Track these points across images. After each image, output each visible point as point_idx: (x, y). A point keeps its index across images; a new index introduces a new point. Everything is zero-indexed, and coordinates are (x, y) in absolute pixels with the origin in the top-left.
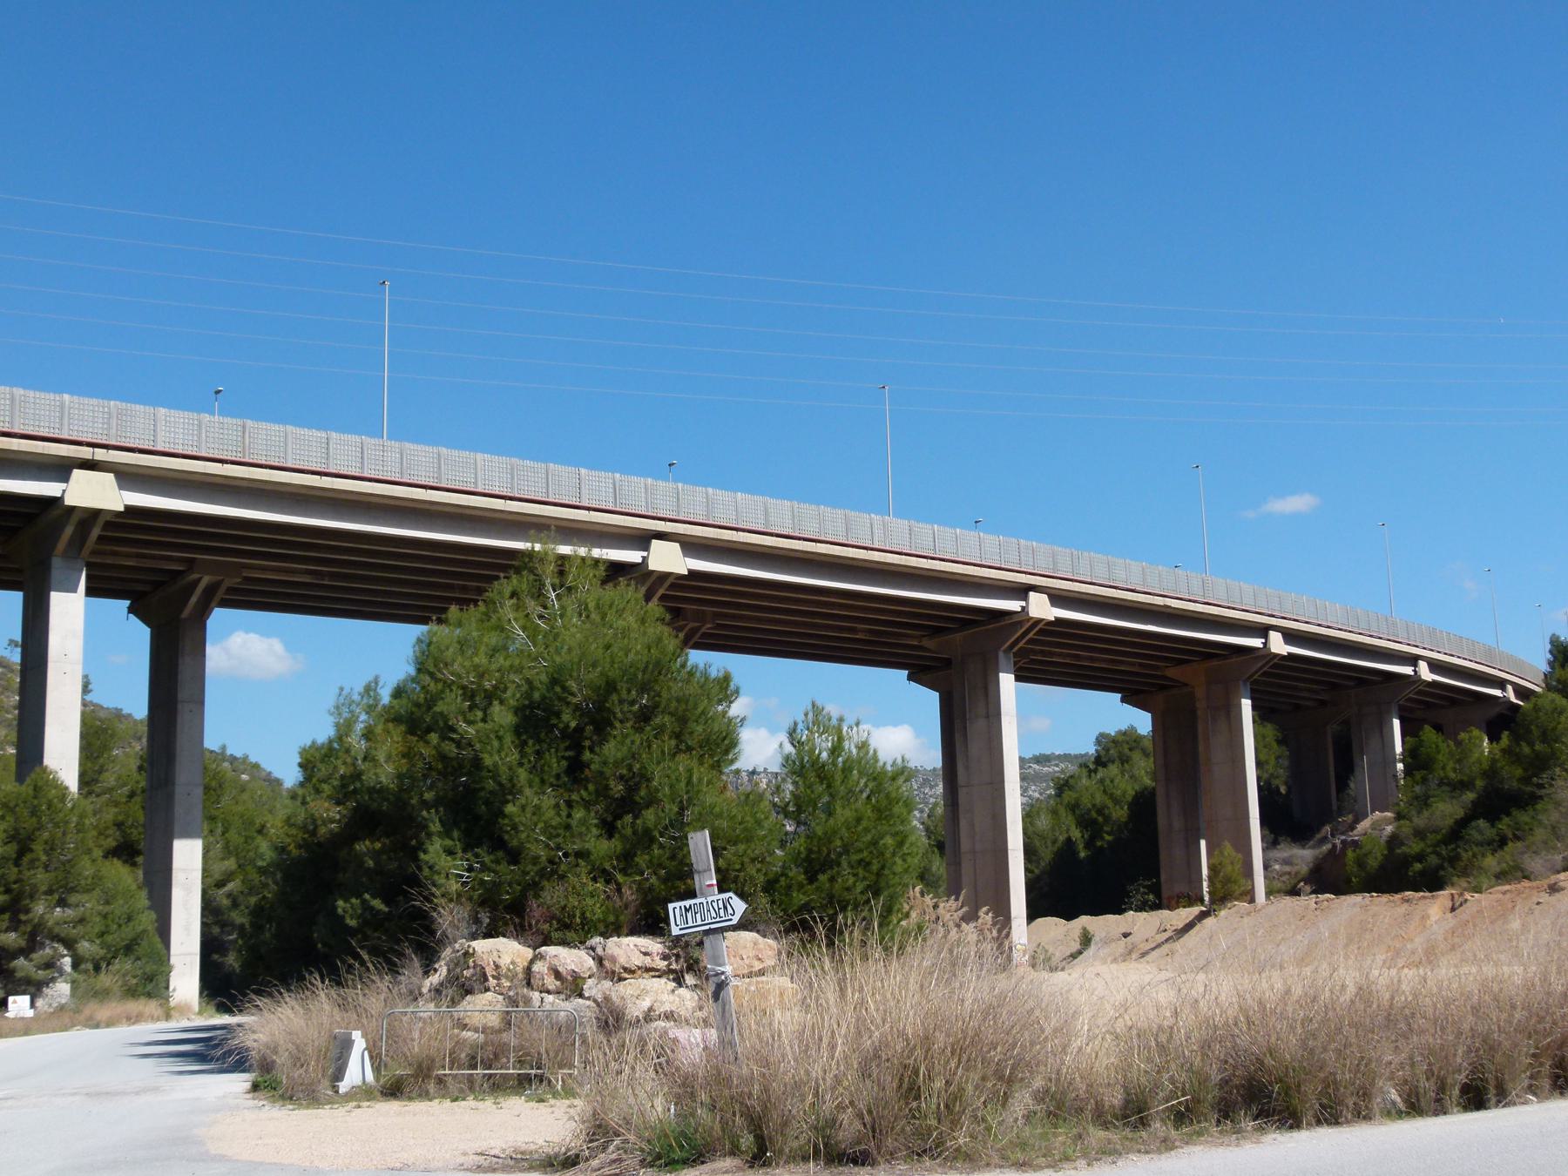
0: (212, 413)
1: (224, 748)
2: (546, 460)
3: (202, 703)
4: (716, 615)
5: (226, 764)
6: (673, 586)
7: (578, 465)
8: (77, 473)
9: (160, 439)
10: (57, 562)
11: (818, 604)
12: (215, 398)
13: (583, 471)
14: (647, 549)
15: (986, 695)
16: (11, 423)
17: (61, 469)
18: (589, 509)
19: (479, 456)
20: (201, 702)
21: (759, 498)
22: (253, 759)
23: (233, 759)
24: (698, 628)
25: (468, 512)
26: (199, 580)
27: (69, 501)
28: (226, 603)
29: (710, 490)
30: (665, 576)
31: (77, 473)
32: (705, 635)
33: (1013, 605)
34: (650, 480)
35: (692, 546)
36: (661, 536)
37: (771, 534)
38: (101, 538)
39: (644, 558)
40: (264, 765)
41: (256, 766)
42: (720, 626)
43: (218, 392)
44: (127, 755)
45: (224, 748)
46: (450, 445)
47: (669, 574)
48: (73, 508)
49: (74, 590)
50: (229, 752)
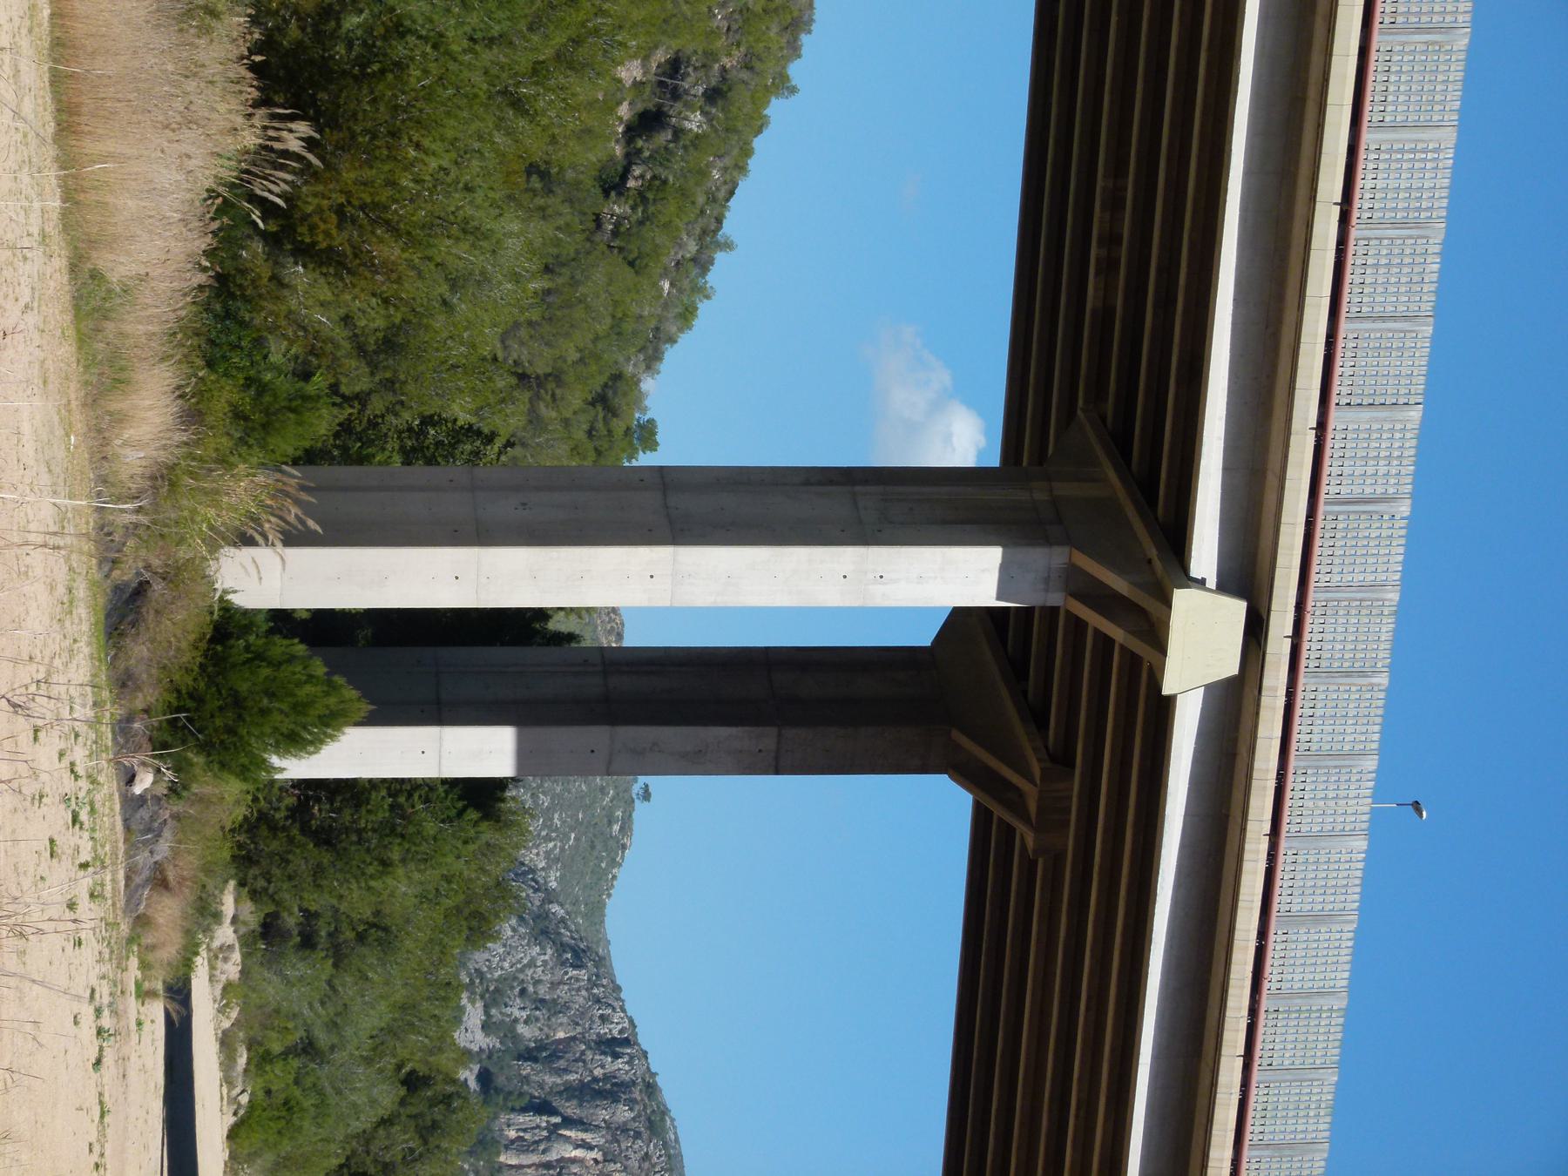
0: (1376, 797)
1: (728, 246)
2: (1438, 313)
3: (777, 773)
4: (1057, 860)
5: (692, 247)
6: (1133, 662)
7: (1433, 399)
8: (1237, 609)
9: (1350, 414)
10: (1056, 557)
11: (1122, 764)
12: (1404, 803)
13: (1416, 414)
14: (1224, 587)
15: (944, 522)
16: (1359, 317)
17: (1246, 576)
18: (1321, 426)
19: (1449, 137)
20: (778, 767)
21: (1353, 900)
22: (703, 307)
23: (702, 263)
24: (1024, 816)
25: (1316, 58)
26: (1027, 775)
27: (1183, 599)
28: (981, 821)
29: (1371, 763)
30: (1156, 636)
31: (1237, 609)
32: (1009, 832)
33: (1205, 555)
34: (1394, 596)
35: (1232, 704)
36: (1256, 629)
37: (1263, 934)
38: (1105, 642)
39: (1201, 583)
40: (685, 339)
41: (687, 315)
42: (1029, 867)
43: (1417, 806)
44: (712, 34)
45: (728, 246)
46: (1359, 936)
47: (1162, 650)
48: (1168, 603)
49: (999, 598)
50: (720, 257)
